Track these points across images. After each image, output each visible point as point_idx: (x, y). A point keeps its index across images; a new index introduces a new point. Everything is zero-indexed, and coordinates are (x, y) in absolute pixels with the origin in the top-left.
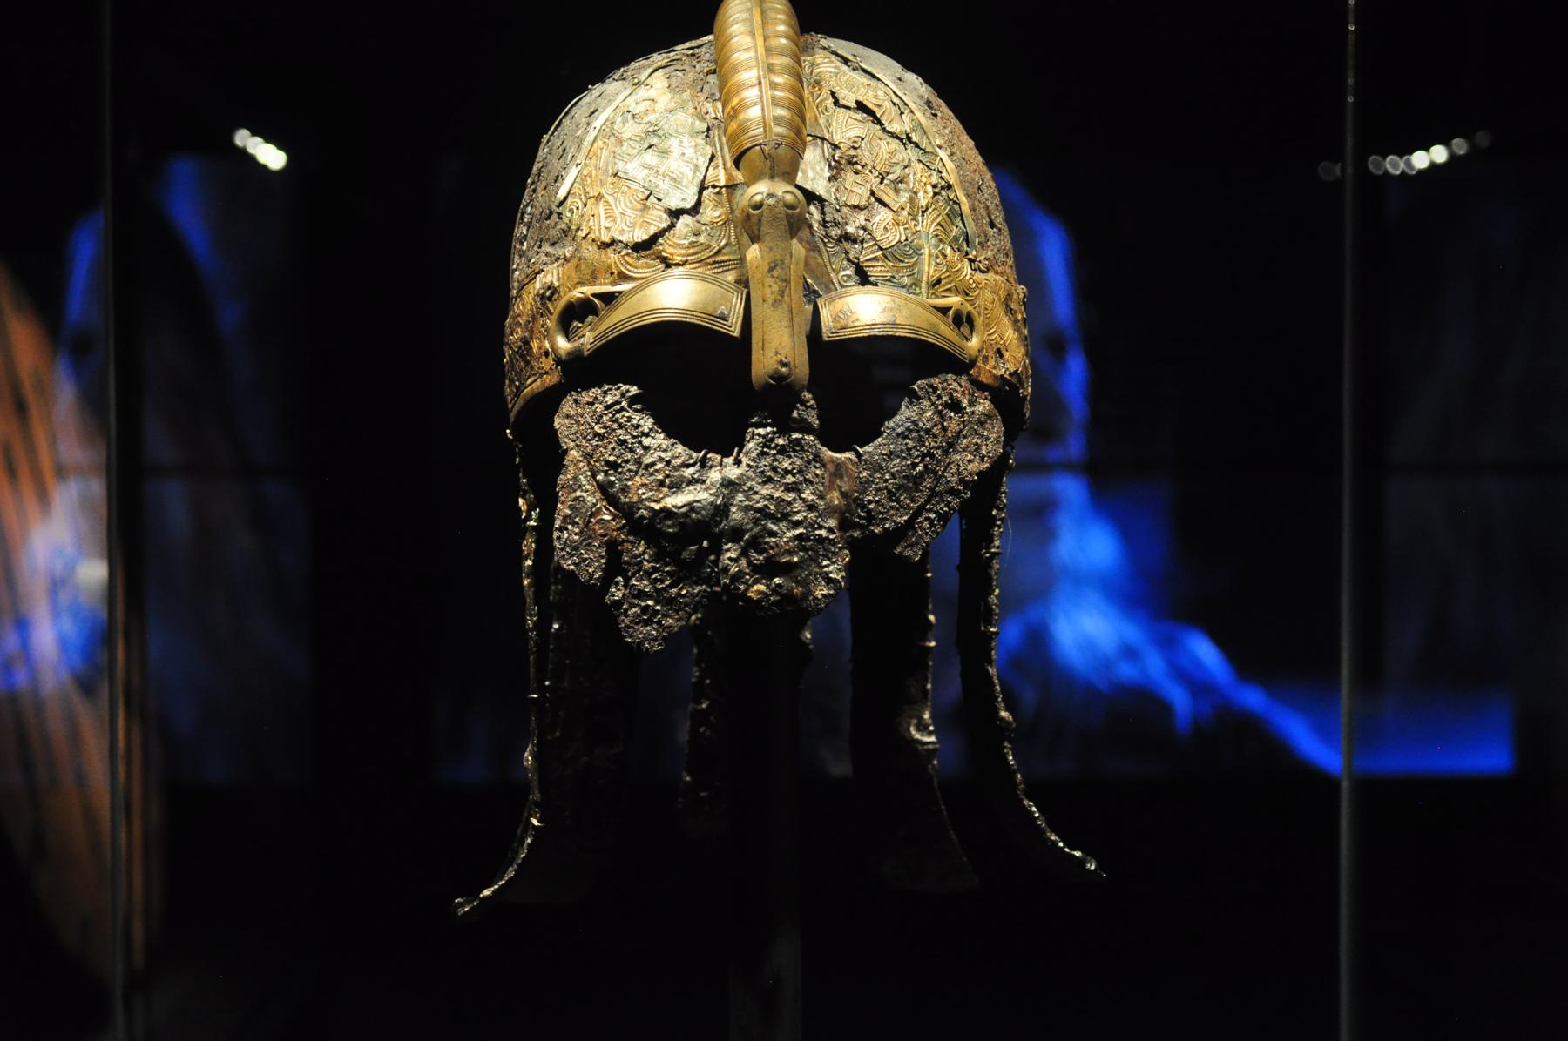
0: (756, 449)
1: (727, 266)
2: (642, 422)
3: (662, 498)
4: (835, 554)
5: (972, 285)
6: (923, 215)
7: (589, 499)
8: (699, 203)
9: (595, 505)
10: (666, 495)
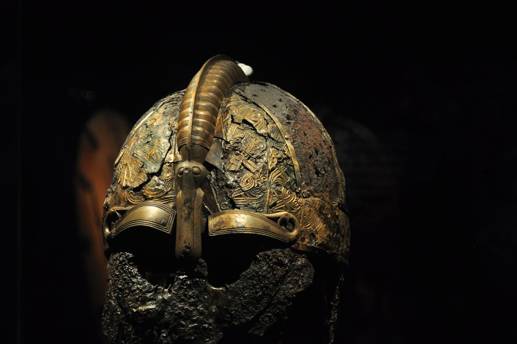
0: (178, 286)
2: (133, 271)
3: (137, 307)
4: (212, 335)
7: (113, 303)
8: (161, 170)
9: (115, 306)
10: (140, 306)
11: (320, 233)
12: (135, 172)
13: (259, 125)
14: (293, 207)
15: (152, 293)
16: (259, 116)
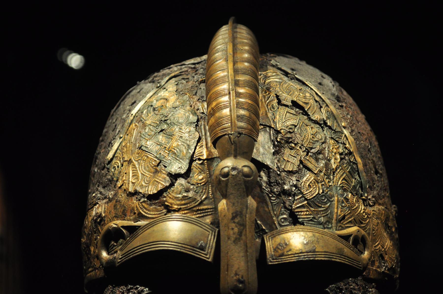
1: (206, 212)
5: (365, 216)
6: (334, 174)
11: (389, 254)
12: (146, 172)
13: (311, 108)
14: (362, 219)
16: (309, 97)
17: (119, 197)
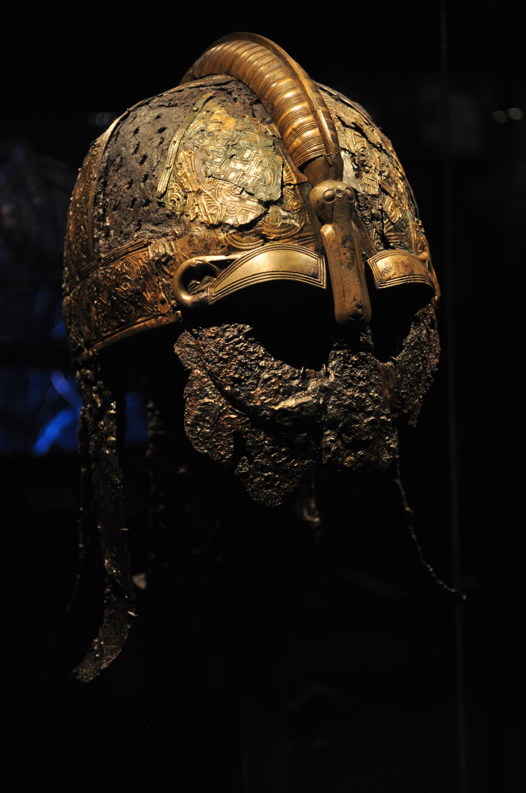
1: (308, 240)
15: (272, 382)
17: (193, 231)
